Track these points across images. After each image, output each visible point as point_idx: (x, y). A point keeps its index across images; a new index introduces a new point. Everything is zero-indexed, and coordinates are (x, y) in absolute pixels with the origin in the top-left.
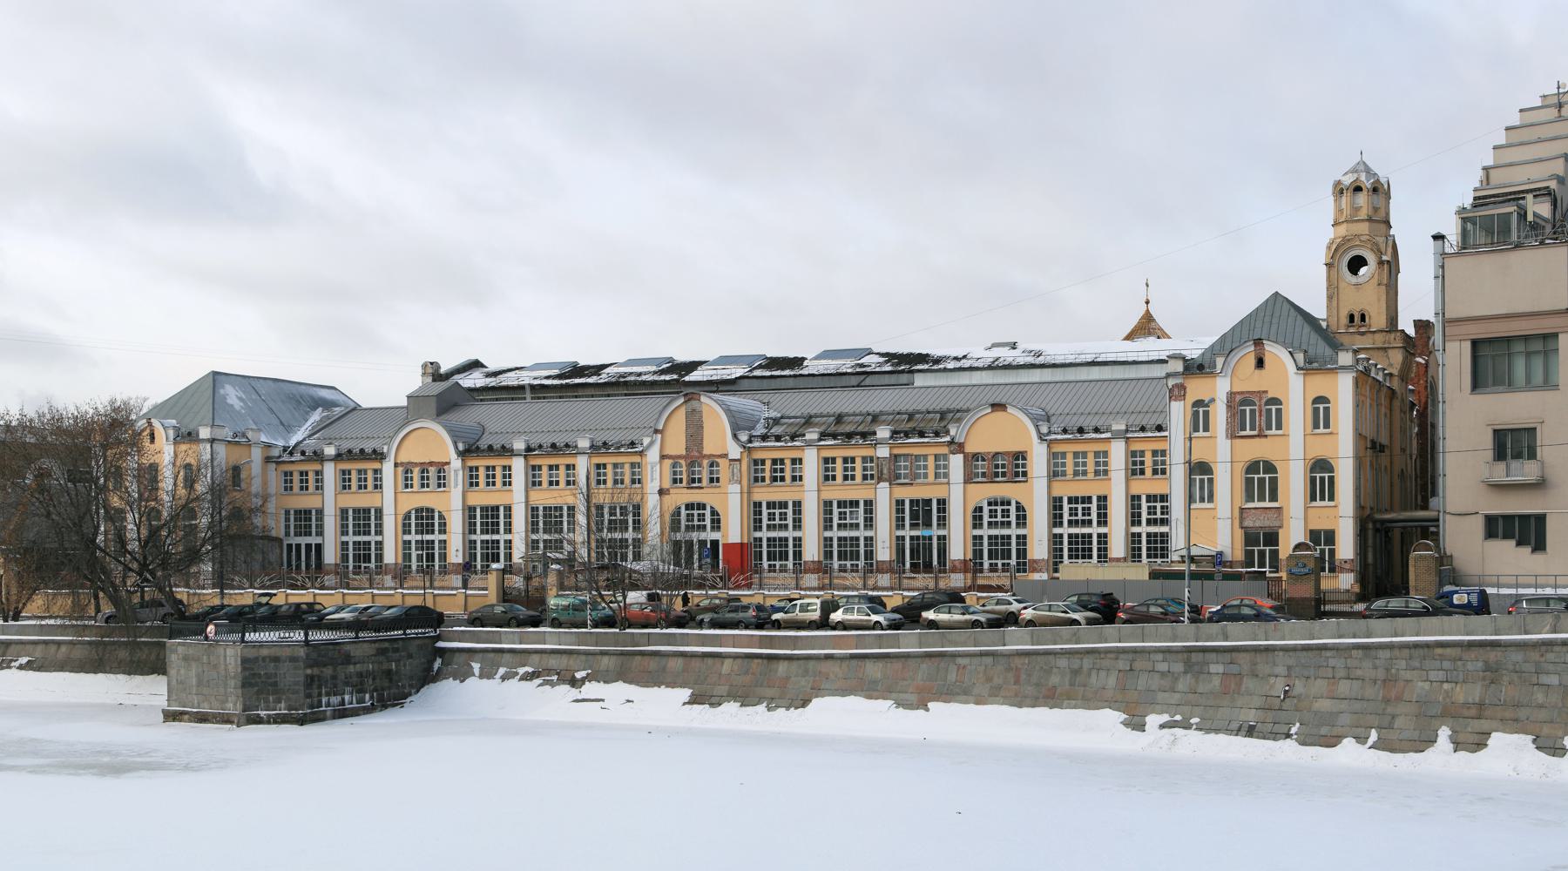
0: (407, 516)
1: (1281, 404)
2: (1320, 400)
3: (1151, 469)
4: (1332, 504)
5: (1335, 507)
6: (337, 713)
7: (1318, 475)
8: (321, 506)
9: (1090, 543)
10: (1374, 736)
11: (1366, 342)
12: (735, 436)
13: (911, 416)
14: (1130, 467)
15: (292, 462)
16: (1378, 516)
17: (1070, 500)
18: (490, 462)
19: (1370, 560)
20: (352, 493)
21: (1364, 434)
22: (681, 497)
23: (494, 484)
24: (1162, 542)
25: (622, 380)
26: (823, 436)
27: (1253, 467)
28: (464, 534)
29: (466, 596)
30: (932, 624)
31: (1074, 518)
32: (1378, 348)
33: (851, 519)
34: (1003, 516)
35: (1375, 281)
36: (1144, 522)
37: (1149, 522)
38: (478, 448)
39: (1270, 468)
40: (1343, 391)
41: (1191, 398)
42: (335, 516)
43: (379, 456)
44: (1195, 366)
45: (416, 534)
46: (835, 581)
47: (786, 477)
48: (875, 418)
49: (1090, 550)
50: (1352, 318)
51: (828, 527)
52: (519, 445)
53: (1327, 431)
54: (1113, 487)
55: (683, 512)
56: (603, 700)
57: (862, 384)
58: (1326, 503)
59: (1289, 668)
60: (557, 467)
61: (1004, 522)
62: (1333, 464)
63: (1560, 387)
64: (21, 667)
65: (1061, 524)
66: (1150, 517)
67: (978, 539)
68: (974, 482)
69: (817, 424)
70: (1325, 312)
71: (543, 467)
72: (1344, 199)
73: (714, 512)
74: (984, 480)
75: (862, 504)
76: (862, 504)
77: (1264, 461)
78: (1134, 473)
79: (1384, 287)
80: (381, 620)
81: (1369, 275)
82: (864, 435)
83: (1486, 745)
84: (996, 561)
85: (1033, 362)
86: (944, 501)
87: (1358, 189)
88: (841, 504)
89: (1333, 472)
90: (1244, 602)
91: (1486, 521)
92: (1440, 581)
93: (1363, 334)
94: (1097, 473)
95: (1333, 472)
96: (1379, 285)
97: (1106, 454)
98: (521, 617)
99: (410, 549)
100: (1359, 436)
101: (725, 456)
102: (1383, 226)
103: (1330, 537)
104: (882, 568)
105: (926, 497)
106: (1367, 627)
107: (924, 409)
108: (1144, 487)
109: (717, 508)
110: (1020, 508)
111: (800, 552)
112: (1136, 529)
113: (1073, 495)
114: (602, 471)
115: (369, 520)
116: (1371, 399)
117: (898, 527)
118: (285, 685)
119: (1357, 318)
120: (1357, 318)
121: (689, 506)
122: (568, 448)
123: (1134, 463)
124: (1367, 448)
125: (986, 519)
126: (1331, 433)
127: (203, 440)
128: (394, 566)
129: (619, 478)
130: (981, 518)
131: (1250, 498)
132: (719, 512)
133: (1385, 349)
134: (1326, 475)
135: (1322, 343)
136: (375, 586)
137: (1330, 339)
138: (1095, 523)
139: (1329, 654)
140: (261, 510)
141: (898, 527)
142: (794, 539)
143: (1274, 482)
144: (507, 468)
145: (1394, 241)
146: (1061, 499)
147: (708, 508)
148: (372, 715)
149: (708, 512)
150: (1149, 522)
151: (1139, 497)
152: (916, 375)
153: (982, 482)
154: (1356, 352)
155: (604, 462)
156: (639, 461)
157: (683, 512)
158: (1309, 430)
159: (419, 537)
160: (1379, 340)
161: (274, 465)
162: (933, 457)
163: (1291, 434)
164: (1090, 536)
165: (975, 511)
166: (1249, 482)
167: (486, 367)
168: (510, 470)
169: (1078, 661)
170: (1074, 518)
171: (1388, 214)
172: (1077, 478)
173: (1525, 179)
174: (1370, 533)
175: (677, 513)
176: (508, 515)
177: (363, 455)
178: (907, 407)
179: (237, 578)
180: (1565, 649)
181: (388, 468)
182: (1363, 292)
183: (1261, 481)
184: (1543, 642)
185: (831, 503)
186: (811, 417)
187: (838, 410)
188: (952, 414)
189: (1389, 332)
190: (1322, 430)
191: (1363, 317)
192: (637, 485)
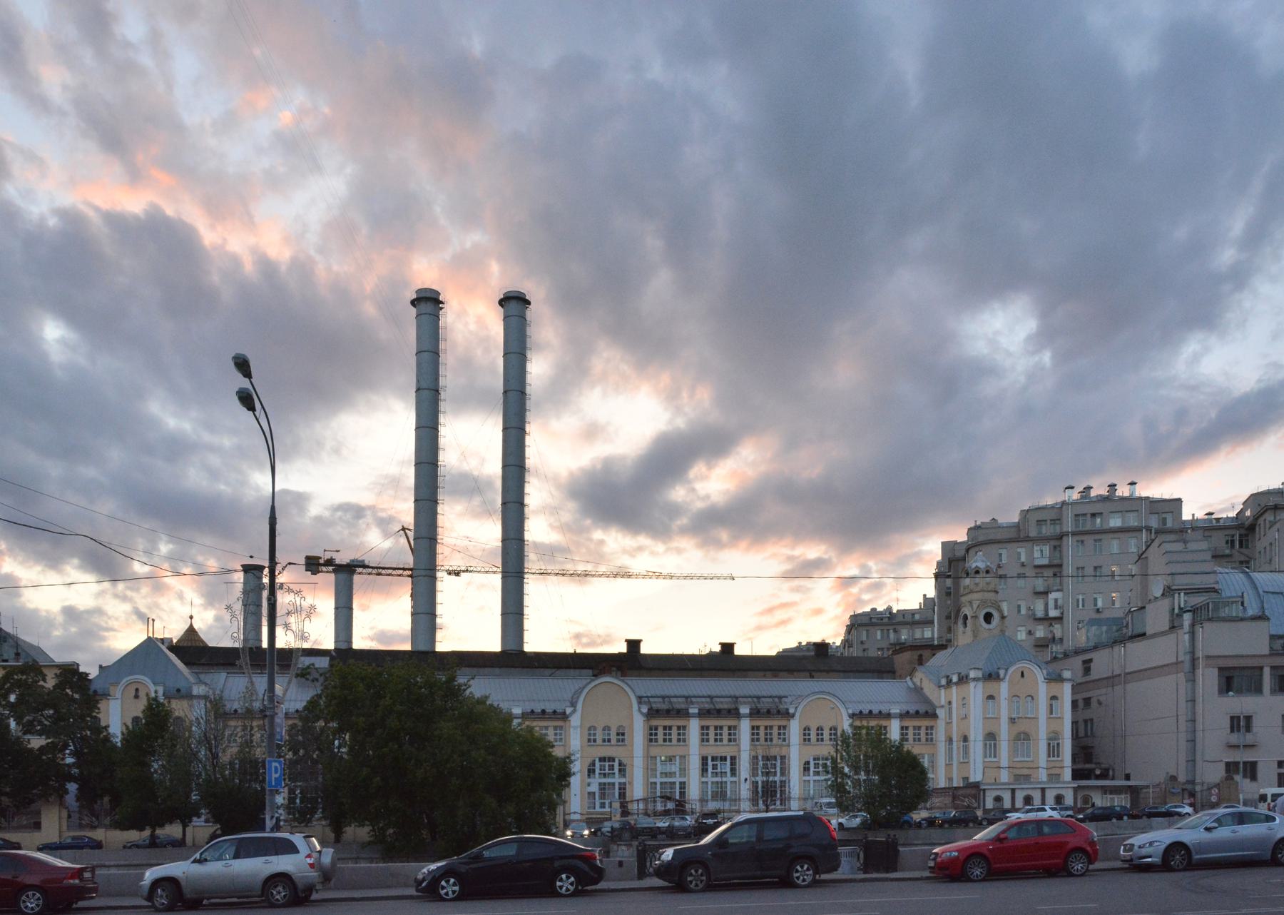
3: (1070, 769)
4: (995, 760)
5: (967, 762)
7: (988, 742)
8: (1199, 631)
10: (262, 816)
12: (639, 710)
14: (737, 732)
18: (768, 723)
20: (723, 745)
23: (708, 740)
26: (1130, 597)
28: (789, 781)
31: (611, 763)
42: (689, 770)
43: (788, 715)
57: (407, 531)
58: (1056, 759)
60: (670, 728)
68: (1225, 620)
74: (561, 744)
75: (728, 759)
76: (728, 759)
77: (1024, 733)
78: (651, 740)
83: (1243, 504)
88: (714, 759)
90: (1098, 671)
91: (710, 891)
92: (889, 672)
98: (552, 489)
106: (1169, 575)
109: (625, 761)
111: (684, 792)
113: (603, 755)
114: (719, 732)
118: (24, 902)
122: (888, 716)
125: (812, 769)
129: (719, 737)
130: (809, 769)
142: (680, 783)
146: (707, 758)
149: (616, 764)
152: (1007, 766)
155: (907, 725)
158: (1049, 716)
159: (724, 779)
162: (727, 728)
164: (674, 783)
165: (805, 764)
170: (611, 763)
177: (769, 714)
180: (1275, 877)
181: (795, 728)
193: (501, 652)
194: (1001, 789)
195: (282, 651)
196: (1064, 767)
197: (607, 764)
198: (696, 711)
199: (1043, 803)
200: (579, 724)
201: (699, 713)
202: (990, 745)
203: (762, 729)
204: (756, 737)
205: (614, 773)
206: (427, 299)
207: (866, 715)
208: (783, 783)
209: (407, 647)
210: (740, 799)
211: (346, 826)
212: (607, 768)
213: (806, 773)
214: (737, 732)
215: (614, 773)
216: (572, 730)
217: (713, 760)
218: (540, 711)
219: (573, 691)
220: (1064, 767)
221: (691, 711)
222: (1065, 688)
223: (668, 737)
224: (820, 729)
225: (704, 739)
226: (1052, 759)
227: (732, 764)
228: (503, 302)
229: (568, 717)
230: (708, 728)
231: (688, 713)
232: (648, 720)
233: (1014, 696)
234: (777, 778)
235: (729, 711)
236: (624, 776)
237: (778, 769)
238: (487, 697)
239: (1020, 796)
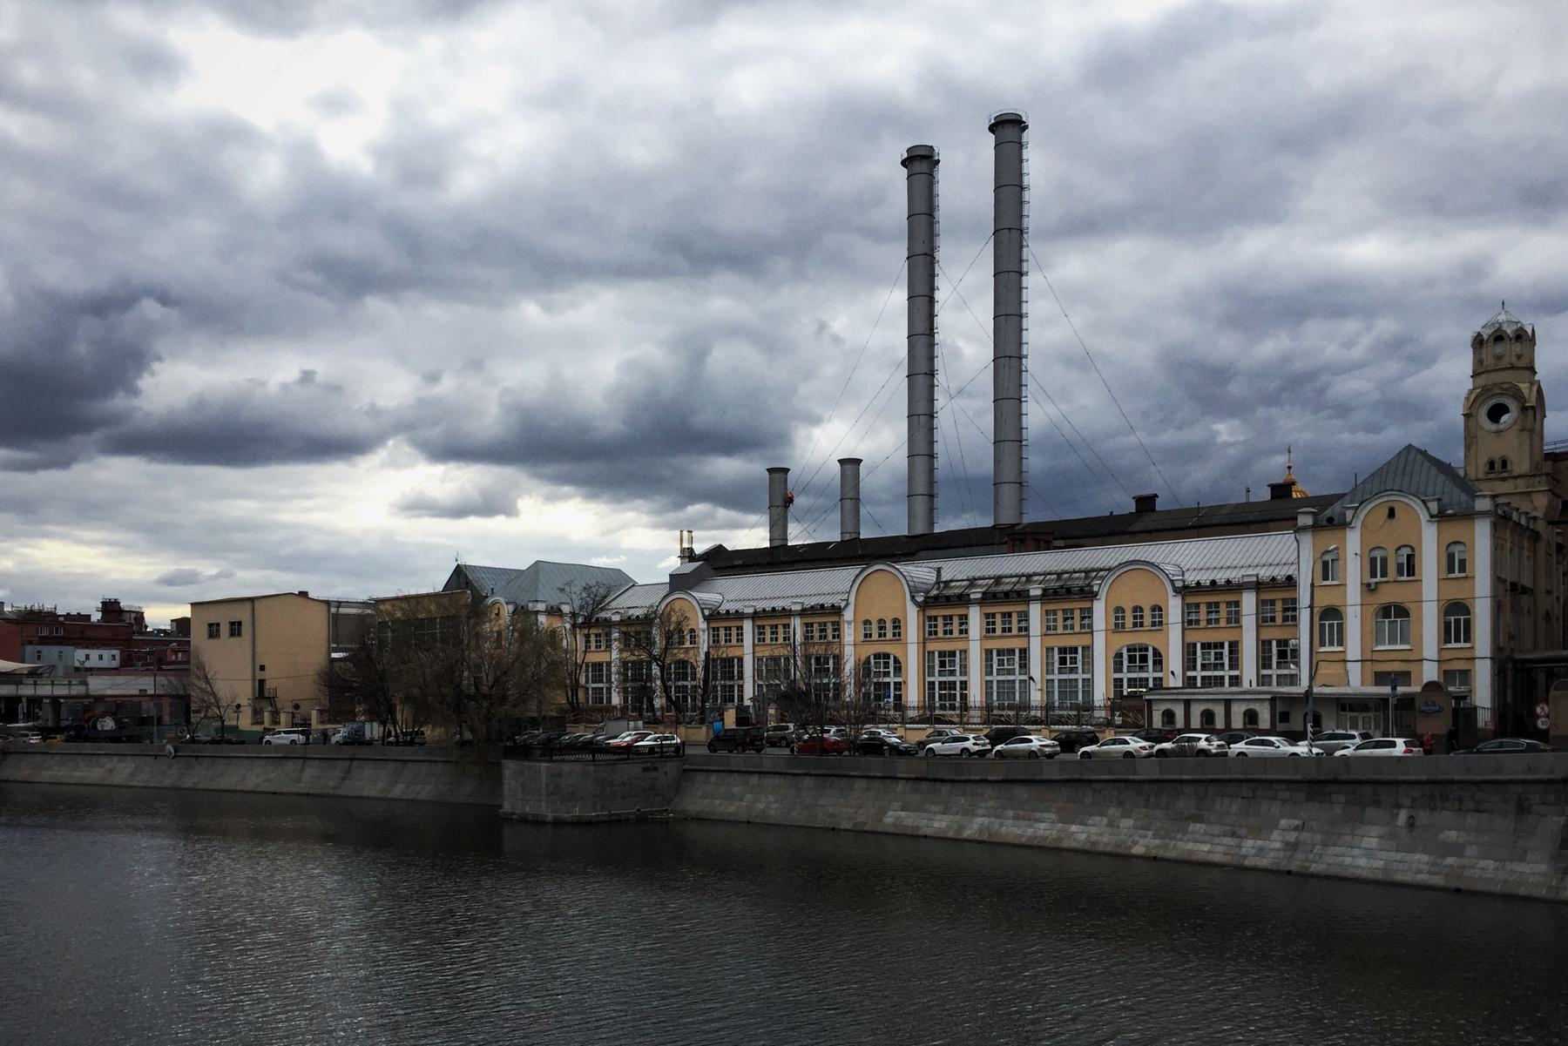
0: (1119, 655)
4: (1468, 645)
5: (1472, 648)
11: (1507, 487)
12: (913, 598)
13: (1059, 575)
16: (1518, 656)
17: (1204, 646)
19: (1509, 699)
20: (601, 651)
21: (1503, 577)
22: (870, 650)
29: (1183, 576)
30: (990, 578)
32: (1521, 493)
33: (1009, 665)
35: (1516, 427)
37: (1204, 667)
38: (719, 613)
40: (1481, 537)
41: (263, 727)
44: (1325, 519)
45: (889, 683)
48: (1029, 577)
50: (1492, 464)
51: (931, 674)
53: (1463, 575)
54: (1244, 633)
59: (1413, 800)
62: (1468, 604)
64: (832, 543)
67: (989, 684)
69: (1008, 583)
70: (1039, 631)
72: (1484, 350)
73: (896, 661)
75: (1017, 651)
76: (1017, 651)
77: (1395, 606)
78: (1265, 620)
79: (1197, 506)
81: (1510, 421)
82: (1019, 593)
87: (16, 970)
88: (1204, 646)
89: (1469, 614)
93: (1504, 479)
94: (1285, 619)
95: (1469, 614)
96: (1522, 430)
99: (1122, 686)
100: (1497, 580)
102: (1527, 373)
103: (1466, 676)
104: (308, 739)
107: (1072, 570)
108: (1273, 634)
110: (1157, 653)
115: (955, 689)
116: (1511, 542)
119: (1498, 466)
120: (1498, 466)
121: (877, 656)
124: (1506, 591)
126: (1467, 577)
131: (1373, 575)
132: (1161, 651)
133: (1529, 493)
135: (1457, 491)
137: (1467, 486)
139: (1455, 787)
140: (1353, 835)
144: (740, 628)
145: (1539, 387)
146: (1195, 645)
147: (1151, 649)
149: (1150, 654)
150: (1204, 667)
151: (933, 652)
152: (1436, 659)
153: (1271, 626)
154: (1494, 497)
156: (837, 620)
160: (1521, 486)
161: (1024, 474)
163: (940, 220)
164: (955, 682)
168: (742, 630)
169: (972, 713)
171: (1532, 360)
172: (1286, 623)
174: (1510, 673)
175: (868, 661)
176: (741, 666)
178: (1098, 565)
181: (1099, 608)
184: (903, 755)
185: (991, 651)
186: (975, 579)
187: (971, 575)
188: (1095, 573)
189: (1534, 476)
190: (1457, 574)
191: (1504, 464)
192: (836, 640)
193: (771, 547)
194: (1260, 699)
196: (1475, 658)
197: (1213, 652)
198: (1039, 592)
199: (276, 722)
200: (852, 618)
201: (982, 598)
202: (1331, 626)
204: (1138, 621)
206: (922, 157)
207: (1221, 586)
208: (898, 686)
209: (767, 545)
210: (1029, 707)
213: (1158, 667)
215: (889, 672)
216: (846, 624)
217: (1060, 652)
219: (1137, 559)
220: (1475, 658)
221: (1032, 593)
222: (1477, 529)
224: (881, 621)
225: (989, 630)
227: (1231, 652)
228: (992, 129)
229: (1096, 595)
230: (994, 615)
231: (970, 600)
232: (924, 611)
233: (1399, 549)
235: (1082, 590)
237: (1079, 665)
238: (1111, 513)
239: (1196, 711)
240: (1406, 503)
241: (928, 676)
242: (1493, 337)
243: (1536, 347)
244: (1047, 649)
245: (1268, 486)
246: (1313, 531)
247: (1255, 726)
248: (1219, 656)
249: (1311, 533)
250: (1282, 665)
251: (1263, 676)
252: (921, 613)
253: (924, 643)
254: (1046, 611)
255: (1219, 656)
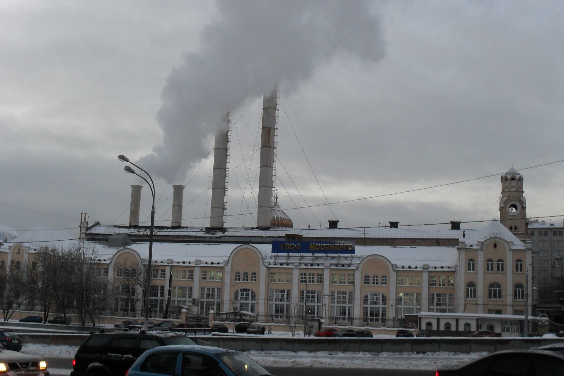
1: (522, 262)
2: (519, 260)
6: (406, 310)
9: (248, 306)
14: (331, 280)
15: (517, 274)
17: (338, 293)
20: (494, 273)
24: (278, 308)
25: (89, 327)
27: (492, 285)
34: (246, 296)
36: (336, 302)
39: (498, 285)
42: (354, 299)
46: (541, 243)
47: (315, 281)
49: (158, 293)
51: (271, 300)
52: (315, 283)
55: (240, 292)
56: (82, 213)
58: (497, 299)
60: (313, 275)
61: (343, 301)
63: (278, 129)
65: (334, 303)
66: (248, 292)
67: (365, 309)
71: (186, 271)
73: (253, 293)
75: (316, 292)
76: (448, 295)
80: (390, 245)
84: (341, 295)
85: (266, 231)
86: (352, 292)
97: (164, 271)
101: (138, 322)
105: (248, 288)
112: (333, 305)
117: (365, 303)
123: (302, 278)
127: (529, 234)
128: (296, 330)
134: (473, 288)
136: (355, 325)
138: (347, 302)
141: (365, 303)
143: (500, 291)
148: (560, 343)
149: (250, 293)
150: (437, 305)
157: (240, 292)
162: (308, 275)
164: (248, 304)
165: (365, 297)
166: (490, 291)
167: (521, 240)
173: (215, 245)
179: (410, 323)
182: (429, 328)
183: (495, 291)
191: (516, 228)
195: (390, 225)
196: (506, 305)
197: (245, 293)
203: (316, 275)
205: (249, 298)
211: (102, 323)
212: (342, 297)
214: (331, 280)
217: (338, 293)
218: (408, 267)
223: (191, 273)
226: (470, 299)
234: (316, 304)
236: (385, 304)
240: (502, 244)
241: (270, 301)
242: (511, 178)
243: (523, 182)
244: (202, 288)
245: (389, 222)
246: (465, 250)
247: (449, 330)
248: (247, 295)
249: (464, 251)
250: (242, 298)
251: (270, 304)
252: (268, 270)
253: (269, 284)
254: (332, 274)
255: (247, 295)
